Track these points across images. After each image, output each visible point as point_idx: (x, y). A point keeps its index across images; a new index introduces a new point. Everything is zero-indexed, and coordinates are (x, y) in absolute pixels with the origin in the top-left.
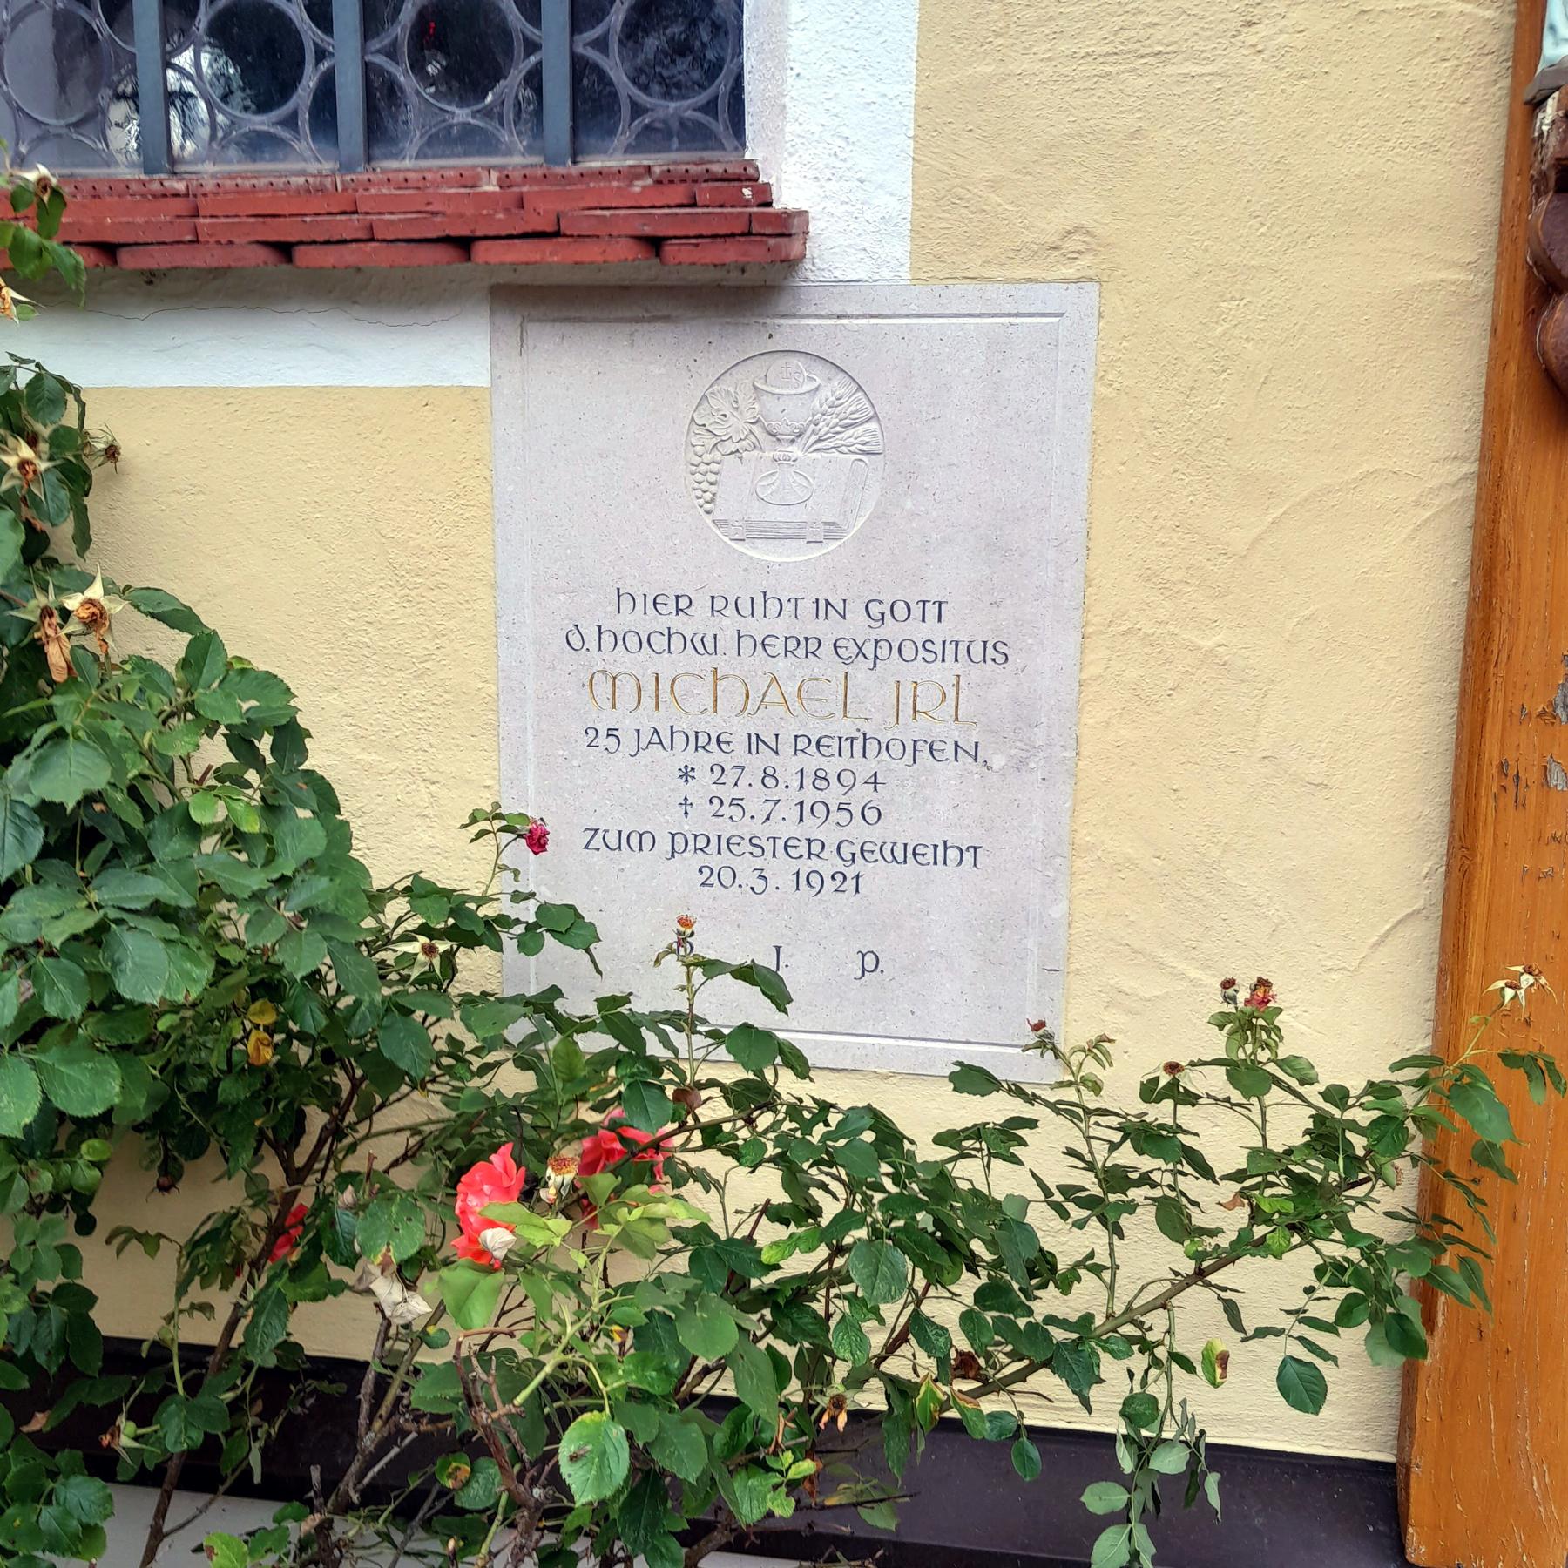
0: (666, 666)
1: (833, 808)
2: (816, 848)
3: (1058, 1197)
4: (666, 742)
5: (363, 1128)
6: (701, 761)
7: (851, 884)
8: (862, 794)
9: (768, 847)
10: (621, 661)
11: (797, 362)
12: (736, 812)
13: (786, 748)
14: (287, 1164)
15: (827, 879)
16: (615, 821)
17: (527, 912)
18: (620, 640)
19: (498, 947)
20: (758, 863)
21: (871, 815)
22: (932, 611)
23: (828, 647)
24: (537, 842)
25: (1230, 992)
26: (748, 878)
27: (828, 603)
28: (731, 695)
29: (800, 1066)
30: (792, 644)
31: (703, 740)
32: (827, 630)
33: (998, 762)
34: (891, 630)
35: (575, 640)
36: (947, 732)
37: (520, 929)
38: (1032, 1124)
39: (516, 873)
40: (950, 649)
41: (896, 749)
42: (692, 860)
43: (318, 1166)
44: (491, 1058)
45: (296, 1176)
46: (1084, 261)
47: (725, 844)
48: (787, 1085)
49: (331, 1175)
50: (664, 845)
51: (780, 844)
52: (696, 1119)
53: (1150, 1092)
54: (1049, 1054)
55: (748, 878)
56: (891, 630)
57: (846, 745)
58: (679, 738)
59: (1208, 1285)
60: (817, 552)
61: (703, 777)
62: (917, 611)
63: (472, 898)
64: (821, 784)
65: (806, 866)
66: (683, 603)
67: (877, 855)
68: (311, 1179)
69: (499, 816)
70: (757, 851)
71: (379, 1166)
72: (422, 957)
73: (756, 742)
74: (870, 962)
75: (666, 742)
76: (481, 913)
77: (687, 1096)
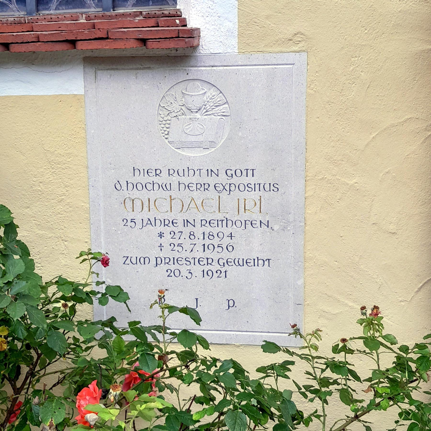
0: (152, 195)
1: (216, 246)
2: (210, 261)
3: (303, 390)
4: (153, 223)
5: (42, 372)
6: (166, 230)
7: (223, 274)
8: (226, 241)
9: (192, 261)
10: (135, 194)
11: (198, 83)
12: (180, 249)
13: (198, 225)
14: (14, 387)
15: (215, 273)
16: (134, 254)
17: (102, 289)
18: (135, 186)
19: (91, 303)
20: (189, 268)
21: (230, 248)
22: (250, 172)
23: (212, 187)
24: (105, 262)
25: (364, 311)
26: (185, 273)
27: (212, 171)
28: (176, 205)
29: (205, 344)
30: (199, 186)
31: (167, 222)
32: (212, 180)
33: (276, 227)
34: (235, 180)
35: (118, 187)
36: (257, 217)
37: (99, 296)
38: (293, 363)
39: (98, 274)
40: (257, 186)
41: (238, 223)
42: (164, 267)
43: (26, 387)
44: (89, 345)
45: (17, 391)
46: (300, 45)
47: (176, 261)
48: (201, 352)
49: (31, 390)
50: (153, 262)
51: (197, 260)
52: (167, 366)
53: (336, 349)
54: (298, 336)
55: (185, 273)
56: (235, 180)
57: (220, 223)
58: (158, 222)
59: (360, 421)
60: (207, 152)
61: (167, 237)
62: (244, 173)
63: (81, 285)
64: (211, 237)
65: (206, 268)
66: (158, 172)
67: (233, 263)
68: (23, 392)
69: (91, 254)
70: (188, 263)
71: (47, 388)
72: (62, 309)
73: (186, 222)
74: (231, 303)
75: (153, 223)
76: (84, 290)
77: (163, 358)
